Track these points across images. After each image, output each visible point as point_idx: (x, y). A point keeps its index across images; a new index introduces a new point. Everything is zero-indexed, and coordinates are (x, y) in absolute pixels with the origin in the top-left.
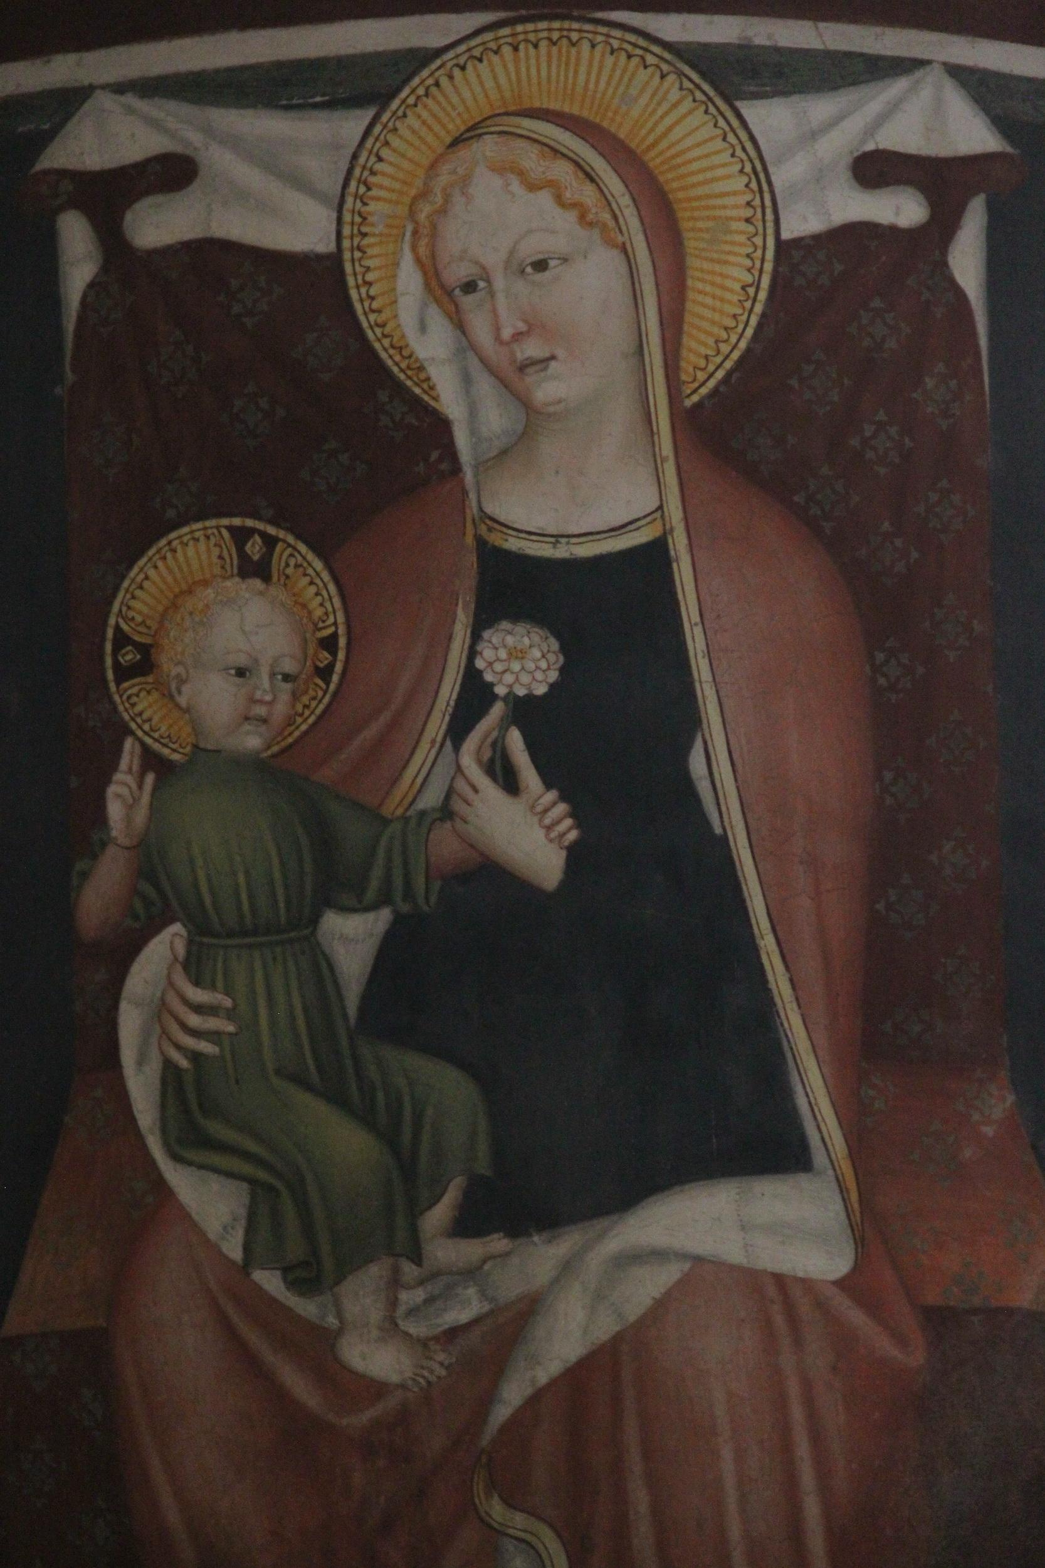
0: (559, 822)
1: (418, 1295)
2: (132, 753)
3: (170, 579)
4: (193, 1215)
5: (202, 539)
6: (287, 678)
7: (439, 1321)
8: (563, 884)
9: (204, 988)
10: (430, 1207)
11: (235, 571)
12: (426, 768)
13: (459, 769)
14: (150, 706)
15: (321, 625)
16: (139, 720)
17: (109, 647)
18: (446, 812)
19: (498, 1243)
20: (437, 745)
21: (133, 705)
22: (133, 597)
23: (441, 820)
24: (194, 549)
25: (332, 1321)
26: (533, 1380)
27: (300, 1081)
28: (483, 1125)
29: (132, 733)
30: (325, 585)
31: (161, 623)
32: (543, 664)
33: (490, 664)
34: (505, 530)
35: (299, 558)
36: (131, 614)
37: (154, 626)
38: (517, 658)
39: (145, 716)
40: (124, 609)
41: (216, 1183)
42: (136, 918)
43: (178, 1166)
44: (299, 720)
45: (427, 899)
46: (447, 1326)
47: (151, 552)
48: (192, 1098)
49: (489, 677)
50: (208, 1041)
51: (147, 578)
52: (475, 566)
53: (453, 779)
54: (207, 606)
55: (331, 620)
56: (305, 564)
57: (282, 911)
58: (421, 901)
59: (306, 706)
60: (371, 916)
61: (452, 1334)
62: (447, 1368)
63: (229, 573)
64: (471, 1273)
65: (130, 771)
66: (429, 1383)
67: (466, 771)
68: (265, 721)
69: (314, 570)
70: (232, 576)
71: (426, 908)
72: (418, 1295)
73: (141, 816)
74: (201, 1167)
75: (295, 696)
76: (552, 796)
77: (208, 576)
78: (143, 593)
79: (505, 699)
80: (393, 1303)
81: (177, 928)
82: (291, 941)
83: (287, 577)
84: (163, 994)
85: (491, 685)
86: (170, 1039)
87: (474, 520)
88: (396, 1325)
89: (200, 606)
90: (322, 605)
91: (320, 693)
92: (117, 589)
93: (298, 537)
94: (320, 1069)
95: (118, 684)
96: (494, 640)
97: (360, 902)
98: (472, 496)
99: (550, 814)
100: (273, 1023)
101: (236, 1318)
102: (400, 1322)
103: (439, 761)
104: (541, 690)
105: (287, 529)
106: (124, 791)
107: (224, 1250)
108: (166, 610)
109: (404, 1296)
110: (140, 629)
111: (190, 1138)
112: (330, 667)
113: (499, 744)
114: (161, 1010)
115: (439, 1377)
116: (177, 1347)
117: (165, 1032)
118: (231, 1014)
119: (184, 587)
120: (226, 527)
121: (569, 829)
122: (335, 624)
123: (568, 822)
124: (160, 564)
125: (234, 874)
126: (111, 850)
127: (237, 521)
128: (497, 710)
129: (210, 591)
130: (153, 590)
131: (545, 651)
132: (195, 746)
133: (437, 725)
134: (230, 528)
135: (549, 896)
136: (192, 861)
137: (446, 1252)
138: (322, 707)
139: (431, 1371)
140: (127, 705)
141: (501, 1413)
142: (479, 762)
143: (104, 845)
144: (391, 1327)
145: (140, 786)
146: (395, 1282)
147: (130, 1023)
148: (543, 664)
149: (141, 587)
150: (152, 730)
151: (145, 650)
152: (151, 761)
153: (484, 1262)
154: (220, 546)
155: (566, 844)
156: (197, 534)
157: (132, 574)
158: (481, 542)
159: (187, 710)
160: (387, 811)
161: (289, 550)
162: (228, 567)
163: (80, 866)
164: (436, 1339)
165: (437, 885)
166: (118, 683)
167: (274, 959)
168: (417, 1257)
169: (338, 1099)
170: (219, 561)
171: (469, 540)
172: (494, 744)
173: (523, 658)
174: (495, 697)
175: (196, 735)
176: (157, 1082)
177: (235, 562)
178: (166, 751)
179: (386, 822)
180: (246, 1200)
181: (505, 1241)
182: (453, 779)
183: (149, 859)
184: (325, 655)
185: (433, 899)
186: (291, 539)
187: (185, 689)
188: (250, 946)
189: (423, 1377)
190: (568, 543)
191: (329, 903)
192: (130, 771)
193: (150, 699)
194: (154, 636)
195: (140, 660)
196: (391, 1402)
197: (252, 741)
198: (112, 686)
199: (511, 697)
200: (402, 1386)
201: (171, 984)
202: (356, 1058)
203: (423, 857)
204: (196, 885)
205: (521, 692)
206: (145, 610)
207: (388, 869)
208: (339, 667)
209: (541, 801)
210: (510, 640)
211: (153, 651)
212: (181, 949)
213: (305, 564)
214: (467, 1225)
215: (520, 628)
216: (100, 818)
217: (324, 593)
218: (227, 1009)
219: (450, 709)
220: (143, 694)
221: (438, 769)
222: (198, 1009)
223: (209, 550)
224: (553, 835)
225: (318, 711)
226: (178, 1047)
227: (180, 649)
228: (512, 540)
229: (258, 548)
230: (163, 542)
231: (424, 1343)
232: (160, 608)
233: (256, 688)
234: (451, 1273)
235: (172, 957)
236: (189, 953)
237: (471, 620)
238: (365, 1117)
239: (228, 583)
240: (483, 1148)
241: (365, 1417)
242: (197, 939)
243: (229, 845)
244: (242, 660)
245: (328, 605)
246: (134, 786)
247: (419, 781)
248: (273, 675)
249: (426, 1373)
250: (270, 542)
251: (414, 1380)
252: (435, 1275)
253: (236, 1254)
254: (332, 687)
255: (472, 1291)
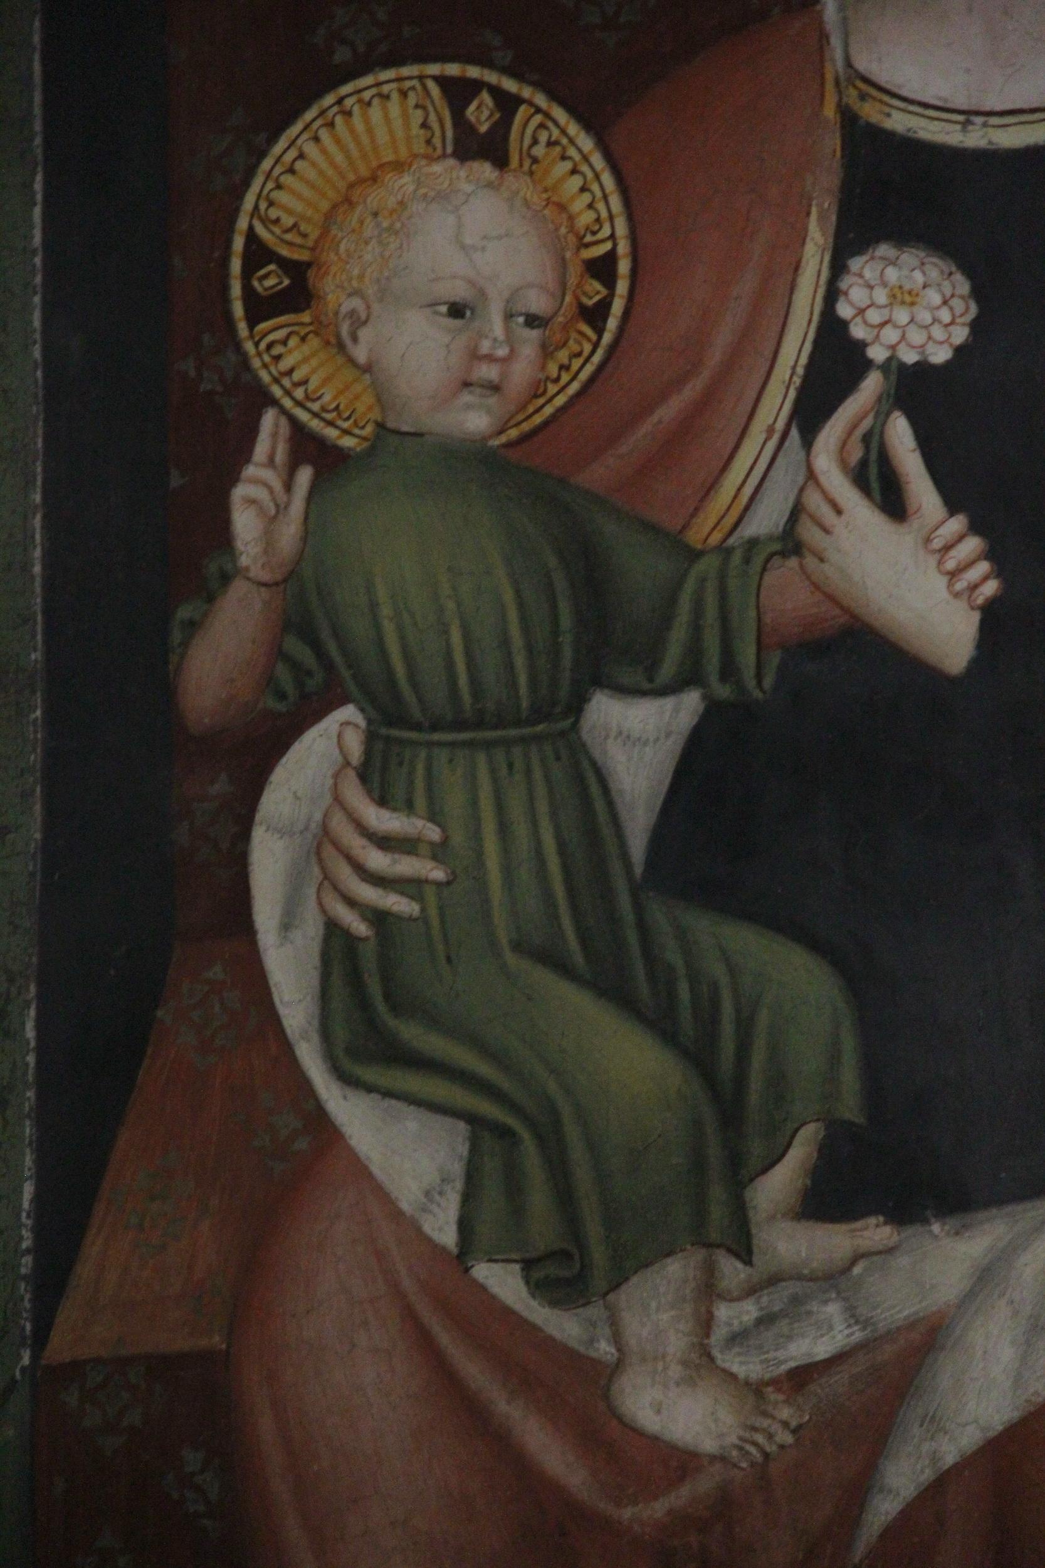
0: (971, 564)
1: (749, 1311)
2: (274, 435)
3: (339, 158)
4: (375, 1170)
5: (395, 96)
6: (532, 321)
7: (781, 1354)
8: (975, 664)
9: (395, 810)
10: (765, 1170)
11: (449, 150)
12: (758, 474)
13: (811, 475)
14: (306, 360)
15: (589, 238)
16: (286, 382)
17: (236, 265)
18: (790, 542)
19: (875, 1232)
20: (776, 437)
21: (277, 358)
22: (279, 187)
23: (784, 554)
24: (383, 113)
25: (605, 1349)
26: (934, 1458)
27: (551, 958)
28: (849, 1044)
29: (275, 402)
30: (611, 218)
31: (325, 232)
32: (945, 315)
33: (861, 312)
34: (886, 98)
35: (556, 133)
36: (273, 213)
37: (314, 234)
38: (903, 303)
39: (297, 376)
40: (263, 206)
41: (413, 1121)
42: (282, 696)
43: (349, 1092)
44: (552, 389)
45: (759, 677)
46: (793, 1364)
47: (309, 115)
48: (381, 1003)
49: (858, 331)
50: (402, 894)
51: (301, 156)
52: (838, 154)
53: (802, 490)
54: (401, 203)
55: (606, 231)
56: (565, 141)
57: (523, 690)
58: (751, 683)
59: (564, 368)
60: (668, 703)
61: (801, 1377)
62: (794, 1432)
63: (439, 151)
64: (834, 1279)
65: (271, 462)
66: (766, 1455)
67: (823, 479)
68: (495, 388)
69: (580, 150)
70: (444, 156)
71: (757, 694)
72: (749, 1311)
73: (290, 532)
74: (388, 1094)
75: (546, 351)
76: (957, 524)
77: (403, 153)
78: (294, 182)
79: (885, 368)
80: (706, 1323)
81: (348, 712)
82: (538, 738)
83: (535, 160)
84: (326, 815)
85: (862, 345)
86: (335, 888)
87: (837, 83)
88: (712, 1359)
89: (392, 202)
90: (590, 206)
91: (587, 348)
92: (250, 172)
93: (553, 96)
94: (584, 941)
95: (251, 326)
96: (868, 274)
97: (651, 680)
98: (836, 42)
99: (953, 553)
100: (508, 871)
101: (445, 1339)
102: (716, 1353)
103: (780, 460)
104: (940, 356)
105: (535, 84)
106: (261, 494)
107: (427, 1228)
108: (335, 206)
109: (723, 1312)
110: (288, 237)
111: (371, 1047)
112: (604, 307)
113: (876, 438)
114: (321, 844)
115: (782, 1447)
116: (345, 1380)
117: (328, 879)
118: (439, 852)
119: (364, 172)
120: (435, 78)
121: (985, 579)
122: (612, 236)
123: (984, 567)
124: (324, 134)
125: (446, 632)
126: (238, 589)
127: (453, 69)
128: (872, 384)
129: (407, 179)
130: (312, 174)
131: (948, 294)
132: (380, 425)
133: (777, 403)
134: (443, 81)
135: (952, 681)
136: (374, 606)
137: (792, 1243)
138: (589, 369)
139: (770, 1437)
140: (267, 358)
141: (883, 1509)
142: (843, 463)
143: (226, 579)
144: (702, 1362)
145: (288, 487)
146: (709, 1290)
147: (269, 862)
148: (945, 315)
149: (291, 171)
150: (307, 397)
151: (297, 271)
152: (306, 447)
153: (854, 1261)
154: (424, 108)
155: (980, 601)
156: (386, 89)
157: (278, 149)
158: (849, 118)
159: (367, 369)
160: (695, 537)
161: (538, 118)
162: (437, 141)
163: (184, 612)
164: (774, 1382)
165: (774, 659)
166: (252, 322)
167: (510, 766)
168: (744, 1252)
169: (615, 991)
170: (422, 132)
171: (830, 111)
172: (866, 439)
173: (913, 304)
174: (868, 364)
175: (383, 410)
176: (316, 960)
177: (450, 134)
178: (331, 433)
179: (694, 555)
180: (464, 1149)
181: (887, 1230)
182: (802, 490)
183: (302, 608)
184: (595, 290)
185: (768, 681)
186: (541, 100)
187: (364, 334)
188: (470, 744)
189: (755, 1444)
190: (985, 125)
191: (599, 682)
192: (271, 462)
193: (306, 349)
194: (313, 249)
195: (288, 287)
196: (704, 1484)
197: (475, 420)
198: (242, 328)
199: (894, 364)
200: (723, 1459)
201: (338, 800)
202: (642, 927)
203: (753, 613)
204: (380, 642)
205: (909, 357)
206: (299, 207)
207: (696, 627)
208: (618, 307)
209: (940, 532)
210: (892, 274)
211: (311, 274)
212: (355, 744)
213: (565, 141)
214: (822, 1202)
215: (910, 257)
216: (221, 535)
217: (595, 188)
218: (432, 844)
219: (797, 381)
220: (293, 342)
221: (777, 473)
222: (384, 842)
223: (405, 116)
224: (959, 586)
225: (584, 375)
226: (351, 902)
227: (356, 272)
228: (896, 115)
229: (486, 113)
230: (329, 99)
231: (756, 1389)
232: (325, 206)
233: (481, 335)
234: (800, 1277)
235: (340, 759)
236: (368, 753)
237: (831, 240)
238: (661, 1024)
239: (437, 168)
240: (850, 1078)
241: (659, 1509)
242: (383, 731)
243: (439, 585)
244: (460, 291)
245: (601, 206)
246: (277, 485)
247: (748, 491)
248: (509, 316)
249: (760, 1438)
250: (507, 104)
251: (741, 1449)
252: (774, 1280)
253: (448, 1237)
254: (607, 338)
255: (833, 1309)
